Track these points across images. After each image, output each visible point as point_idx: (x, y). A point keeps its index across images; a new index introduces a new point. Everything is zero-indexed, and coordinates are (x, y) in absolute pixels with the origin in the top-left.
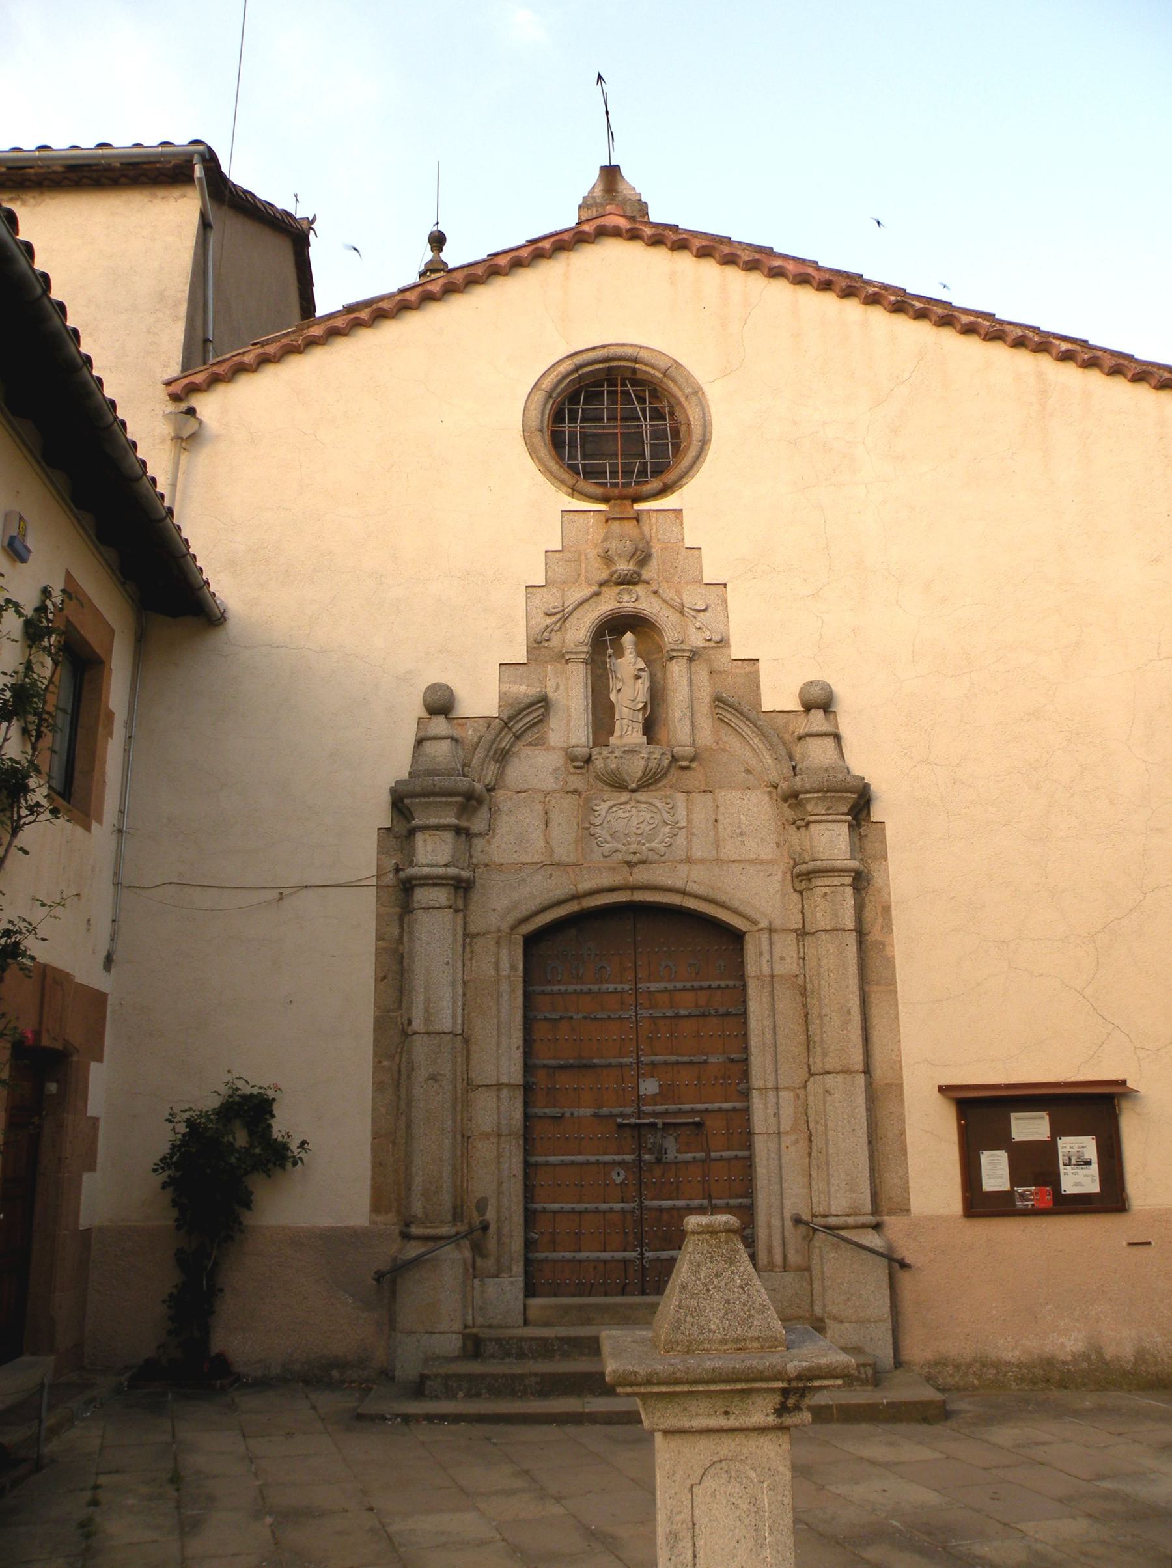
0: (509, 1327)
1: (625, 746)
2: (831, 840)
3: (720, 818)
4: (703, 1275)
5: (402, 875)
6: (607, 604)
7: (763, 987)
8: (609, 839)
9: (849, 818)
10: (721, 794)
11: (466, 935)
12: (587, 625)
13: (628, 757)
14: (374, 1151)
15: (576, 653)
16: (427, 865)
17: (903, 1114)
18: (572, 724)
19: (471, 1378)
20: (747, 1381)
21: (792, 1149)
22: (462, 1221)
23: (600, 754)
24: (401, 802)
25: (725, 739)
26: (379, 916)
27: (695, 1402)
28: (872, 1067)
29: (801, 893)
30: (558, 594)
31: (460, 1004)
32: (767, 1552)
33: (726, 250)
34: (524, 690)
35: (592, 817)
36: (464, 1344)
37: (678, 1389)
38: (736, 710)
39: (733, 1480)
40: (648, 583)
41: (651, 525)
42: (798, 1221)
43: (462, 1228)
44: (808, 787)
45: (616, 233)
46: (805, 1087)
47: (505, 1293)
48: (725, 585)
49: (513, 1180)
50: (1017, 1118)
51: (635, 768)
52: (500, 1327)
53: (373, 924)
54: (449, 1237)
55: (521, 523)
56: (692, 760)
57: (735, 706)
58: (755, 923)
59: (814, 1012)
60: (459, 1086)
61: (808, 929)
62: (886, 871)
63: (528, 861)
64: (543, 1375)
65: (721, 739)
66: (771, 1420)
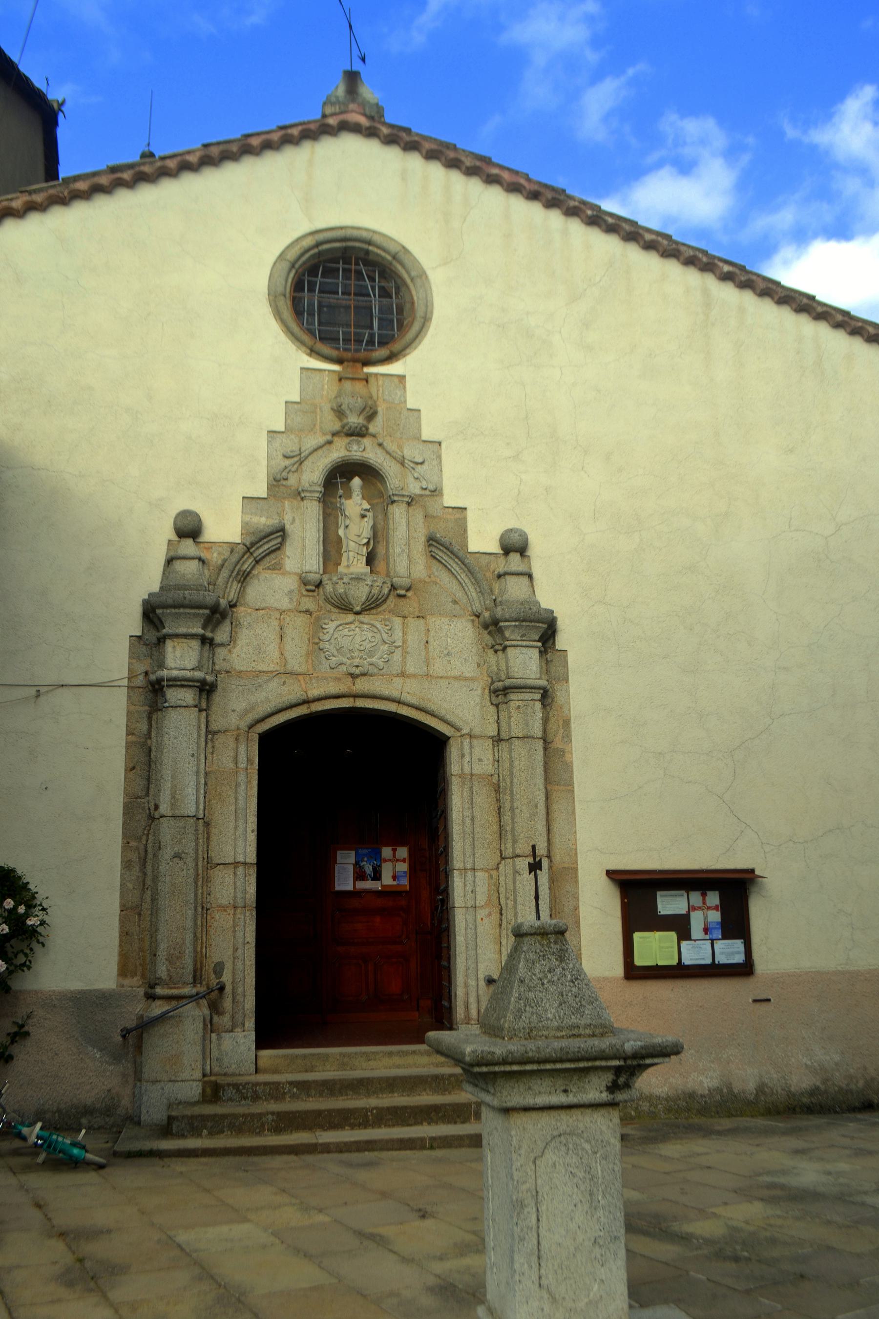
0: (242, 1075)
1: (352, 574)
2: (524, 663)
3: (431, 640)
4: (537, 971)
5: (153, 677)
6: (339, 452)
7: (464, 783)
8: (335, 653)
9: (540, 644)
10: (431, 620)
11: (208, 732)
12: (321, 468)
13: (354, 583)
14: (122, 922)
15: (311, 492)
16: (176, 669)
17: (577, 893)
18: (306, 553)
19: (213, 1117)
20: (588, 1059)
21: (486, 920)
22: (201, 983)
23: (331, 580)
24: (152, 613)
25: (436, 574)
26: (129, 714)
27: (539, 1082)
28: (552, 854)
29: (497, 706)
30: (296, 440)
31: (202, 791)
32: (600, 1213)
33: (452, 155)
34: (263, 521)
35: (321, 634)
36: (204, 1091)
37: (528, 1067)
38: (448, 549)
39: (571, 1152)
40: (374, 436)
41: (378, 386)
43: (201, 989)
44: (507, 617)
45: (356, 129)
46: (497, 869)
47: (239, 1046)
48: (440, 443)
50: (661, 896)
51: (360, 594)
52: (234, 1075)
53: (123, 721)
54: (191, 997)
55: (269, 374)
56: (408, 590)
57: (444, 547)
58: (458, 729)
59: (507, 805)
60: (200, 863)
61: (504, 735)
62: (567, 691)
64: (279, 1114)
65: (433, 573)
66: (605, 1096)
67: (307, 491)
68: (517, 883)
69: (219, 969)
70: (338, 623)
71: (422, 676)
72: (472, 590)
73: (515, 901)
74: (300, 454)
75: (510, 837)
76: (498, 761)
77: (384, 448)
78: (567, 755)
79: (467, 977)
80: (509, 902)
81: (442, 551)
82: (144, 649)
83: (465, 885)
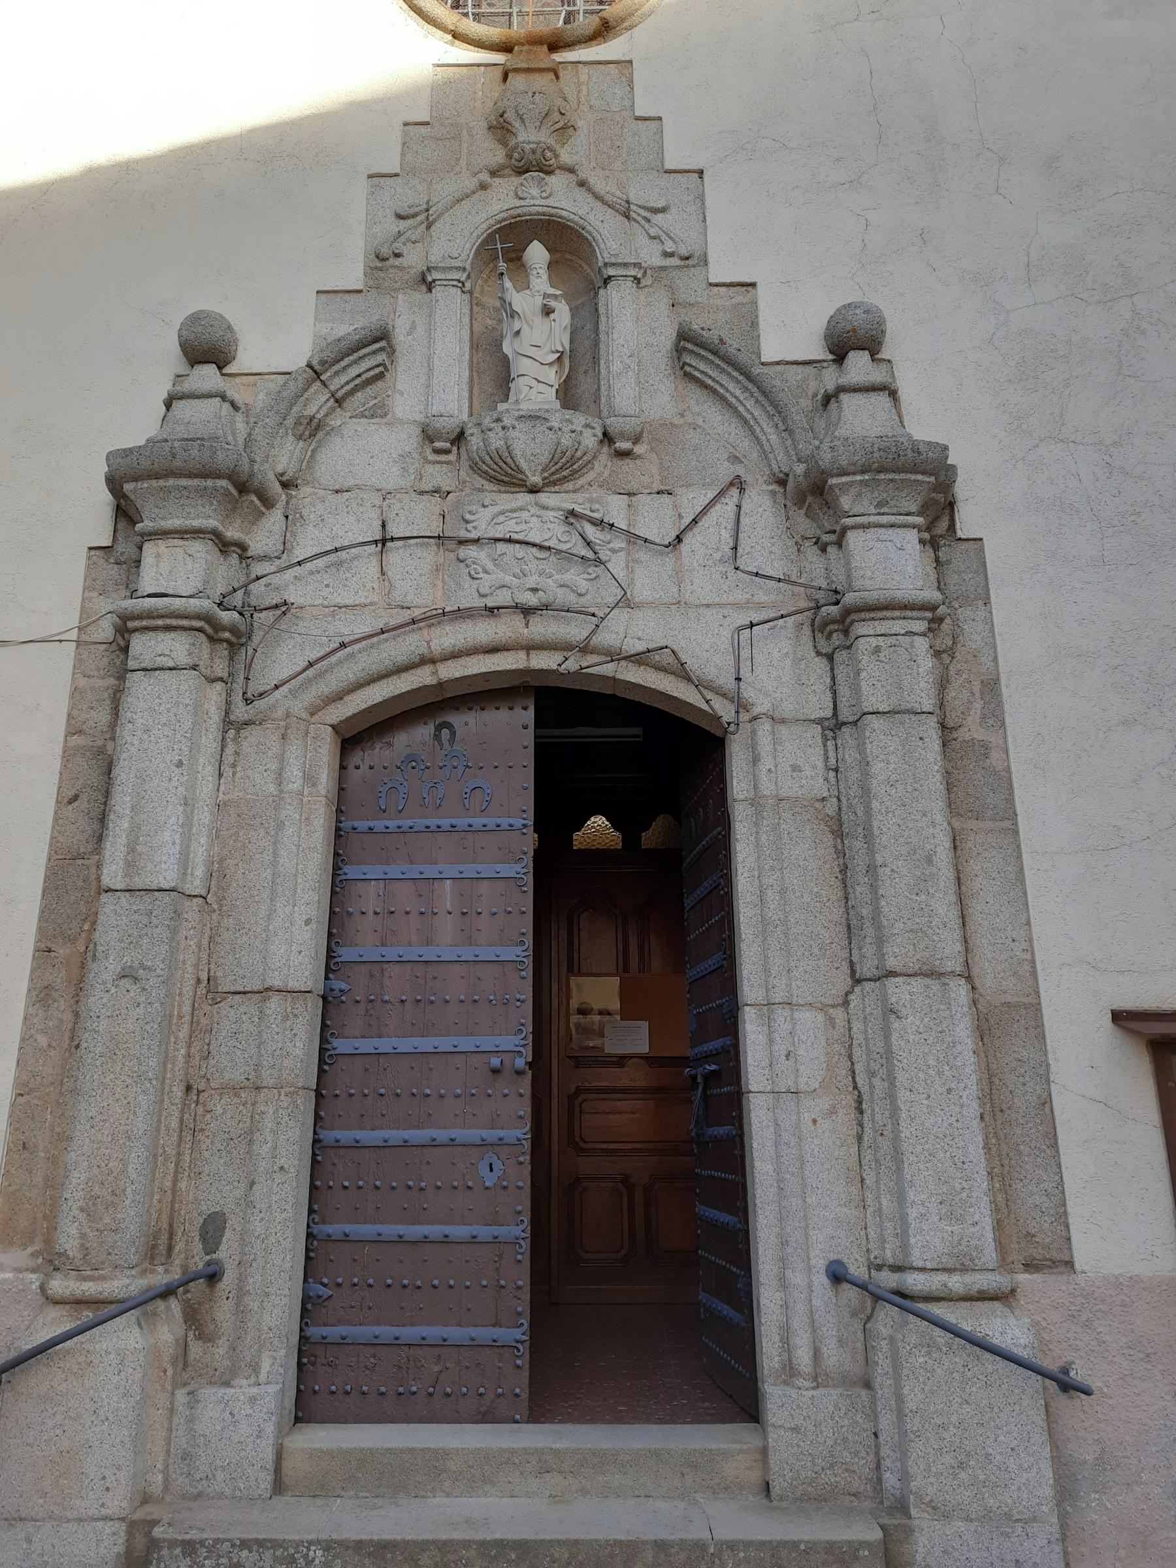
2: (887, 559)
6: (504, 199)
8: (490, 566)
9: (920, 520)
15: (445, 269)
26: (76, 693)
28: (975, 971)
29: (830, 657)
38: (715, 353)
42: (837, 1276)
46: (846, 1003)
48: (701, 173)
49: (278, 1178)
56: (637, 440)
59: (860, 862)
61: (845, 714)
63: (349, 602)
67: (435, 268)
68: (894, 1038)
69: (212, 1229)
70: (497, 509)
71: (668, 605)
72: (769, 429)
73: (891, 1080)
74: (427, 210)
75: (869, 931)
76: (836, 770)
77: (589, 190)
78: (996, 757)
79: (783, 1261)
80: (876, 1081)
81: (702, 357)
82: (114, 571)
83: (771, 1041)
